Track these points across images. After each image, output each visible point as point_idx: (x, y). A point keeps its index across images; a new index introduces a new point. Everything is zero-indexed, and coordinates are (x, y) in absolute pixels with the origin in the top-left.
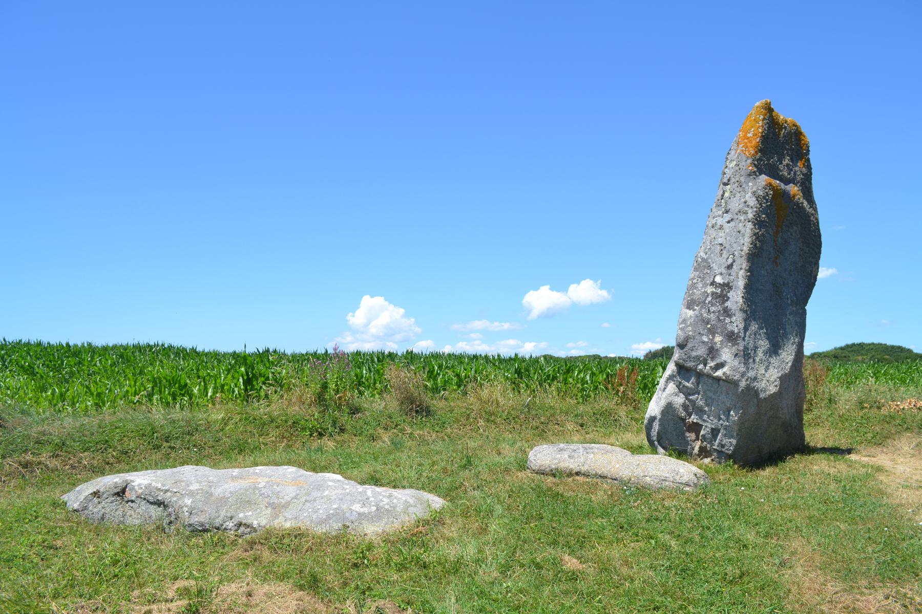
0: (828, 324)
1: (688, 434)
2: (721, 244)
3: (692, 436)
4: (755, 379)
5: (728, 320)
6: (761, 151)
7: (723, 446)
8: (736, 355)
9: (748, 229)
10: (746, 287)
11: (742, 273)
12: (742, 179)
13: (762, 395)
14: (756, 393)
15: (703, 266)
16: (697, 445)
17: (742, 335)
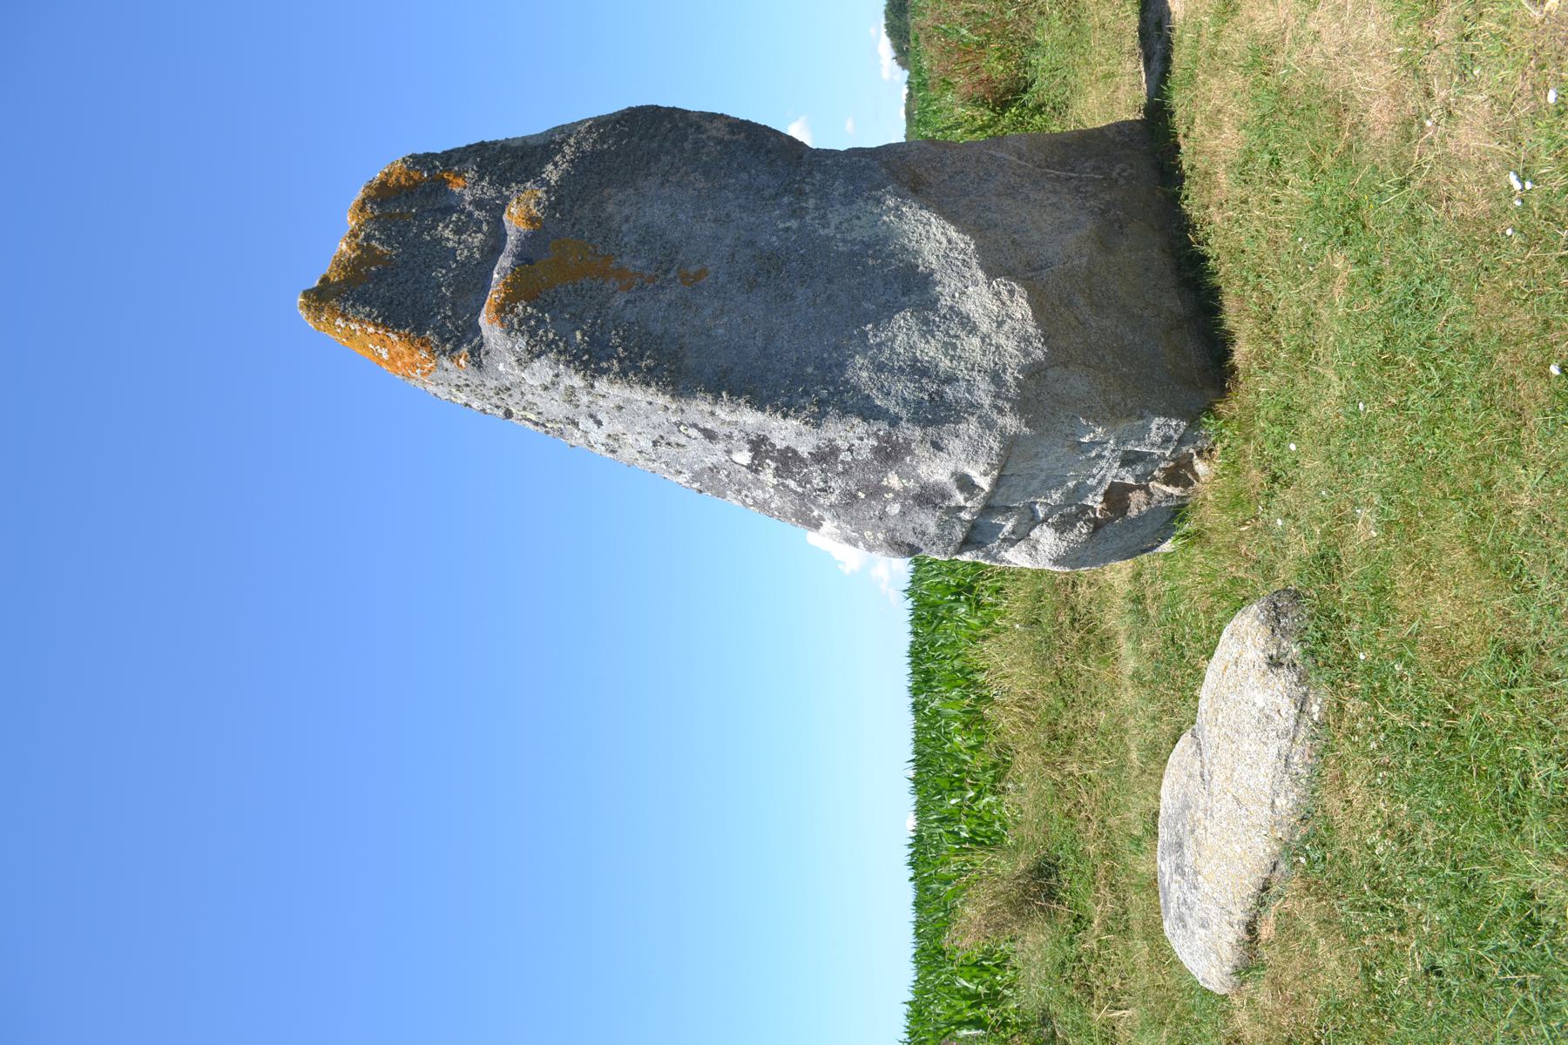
0: (847, 93)
1: (1133, 513)
2: (655, 443)
3: (1137, 498)
4: (996, 378)
5: (845, 456)
6: (419, 329)
7: (1167, 440)
8: (937, 446)
9: (611, 391)
10: (758, 404)
11: (722, 413)
12: (491, 383)
13: (1039, 352)
14: (1033, 372)
15: (710, 480)
16: (1160, 488)
17: (883, 427)
